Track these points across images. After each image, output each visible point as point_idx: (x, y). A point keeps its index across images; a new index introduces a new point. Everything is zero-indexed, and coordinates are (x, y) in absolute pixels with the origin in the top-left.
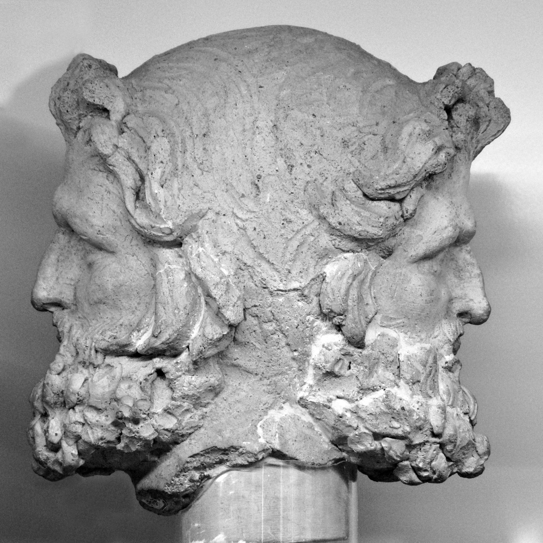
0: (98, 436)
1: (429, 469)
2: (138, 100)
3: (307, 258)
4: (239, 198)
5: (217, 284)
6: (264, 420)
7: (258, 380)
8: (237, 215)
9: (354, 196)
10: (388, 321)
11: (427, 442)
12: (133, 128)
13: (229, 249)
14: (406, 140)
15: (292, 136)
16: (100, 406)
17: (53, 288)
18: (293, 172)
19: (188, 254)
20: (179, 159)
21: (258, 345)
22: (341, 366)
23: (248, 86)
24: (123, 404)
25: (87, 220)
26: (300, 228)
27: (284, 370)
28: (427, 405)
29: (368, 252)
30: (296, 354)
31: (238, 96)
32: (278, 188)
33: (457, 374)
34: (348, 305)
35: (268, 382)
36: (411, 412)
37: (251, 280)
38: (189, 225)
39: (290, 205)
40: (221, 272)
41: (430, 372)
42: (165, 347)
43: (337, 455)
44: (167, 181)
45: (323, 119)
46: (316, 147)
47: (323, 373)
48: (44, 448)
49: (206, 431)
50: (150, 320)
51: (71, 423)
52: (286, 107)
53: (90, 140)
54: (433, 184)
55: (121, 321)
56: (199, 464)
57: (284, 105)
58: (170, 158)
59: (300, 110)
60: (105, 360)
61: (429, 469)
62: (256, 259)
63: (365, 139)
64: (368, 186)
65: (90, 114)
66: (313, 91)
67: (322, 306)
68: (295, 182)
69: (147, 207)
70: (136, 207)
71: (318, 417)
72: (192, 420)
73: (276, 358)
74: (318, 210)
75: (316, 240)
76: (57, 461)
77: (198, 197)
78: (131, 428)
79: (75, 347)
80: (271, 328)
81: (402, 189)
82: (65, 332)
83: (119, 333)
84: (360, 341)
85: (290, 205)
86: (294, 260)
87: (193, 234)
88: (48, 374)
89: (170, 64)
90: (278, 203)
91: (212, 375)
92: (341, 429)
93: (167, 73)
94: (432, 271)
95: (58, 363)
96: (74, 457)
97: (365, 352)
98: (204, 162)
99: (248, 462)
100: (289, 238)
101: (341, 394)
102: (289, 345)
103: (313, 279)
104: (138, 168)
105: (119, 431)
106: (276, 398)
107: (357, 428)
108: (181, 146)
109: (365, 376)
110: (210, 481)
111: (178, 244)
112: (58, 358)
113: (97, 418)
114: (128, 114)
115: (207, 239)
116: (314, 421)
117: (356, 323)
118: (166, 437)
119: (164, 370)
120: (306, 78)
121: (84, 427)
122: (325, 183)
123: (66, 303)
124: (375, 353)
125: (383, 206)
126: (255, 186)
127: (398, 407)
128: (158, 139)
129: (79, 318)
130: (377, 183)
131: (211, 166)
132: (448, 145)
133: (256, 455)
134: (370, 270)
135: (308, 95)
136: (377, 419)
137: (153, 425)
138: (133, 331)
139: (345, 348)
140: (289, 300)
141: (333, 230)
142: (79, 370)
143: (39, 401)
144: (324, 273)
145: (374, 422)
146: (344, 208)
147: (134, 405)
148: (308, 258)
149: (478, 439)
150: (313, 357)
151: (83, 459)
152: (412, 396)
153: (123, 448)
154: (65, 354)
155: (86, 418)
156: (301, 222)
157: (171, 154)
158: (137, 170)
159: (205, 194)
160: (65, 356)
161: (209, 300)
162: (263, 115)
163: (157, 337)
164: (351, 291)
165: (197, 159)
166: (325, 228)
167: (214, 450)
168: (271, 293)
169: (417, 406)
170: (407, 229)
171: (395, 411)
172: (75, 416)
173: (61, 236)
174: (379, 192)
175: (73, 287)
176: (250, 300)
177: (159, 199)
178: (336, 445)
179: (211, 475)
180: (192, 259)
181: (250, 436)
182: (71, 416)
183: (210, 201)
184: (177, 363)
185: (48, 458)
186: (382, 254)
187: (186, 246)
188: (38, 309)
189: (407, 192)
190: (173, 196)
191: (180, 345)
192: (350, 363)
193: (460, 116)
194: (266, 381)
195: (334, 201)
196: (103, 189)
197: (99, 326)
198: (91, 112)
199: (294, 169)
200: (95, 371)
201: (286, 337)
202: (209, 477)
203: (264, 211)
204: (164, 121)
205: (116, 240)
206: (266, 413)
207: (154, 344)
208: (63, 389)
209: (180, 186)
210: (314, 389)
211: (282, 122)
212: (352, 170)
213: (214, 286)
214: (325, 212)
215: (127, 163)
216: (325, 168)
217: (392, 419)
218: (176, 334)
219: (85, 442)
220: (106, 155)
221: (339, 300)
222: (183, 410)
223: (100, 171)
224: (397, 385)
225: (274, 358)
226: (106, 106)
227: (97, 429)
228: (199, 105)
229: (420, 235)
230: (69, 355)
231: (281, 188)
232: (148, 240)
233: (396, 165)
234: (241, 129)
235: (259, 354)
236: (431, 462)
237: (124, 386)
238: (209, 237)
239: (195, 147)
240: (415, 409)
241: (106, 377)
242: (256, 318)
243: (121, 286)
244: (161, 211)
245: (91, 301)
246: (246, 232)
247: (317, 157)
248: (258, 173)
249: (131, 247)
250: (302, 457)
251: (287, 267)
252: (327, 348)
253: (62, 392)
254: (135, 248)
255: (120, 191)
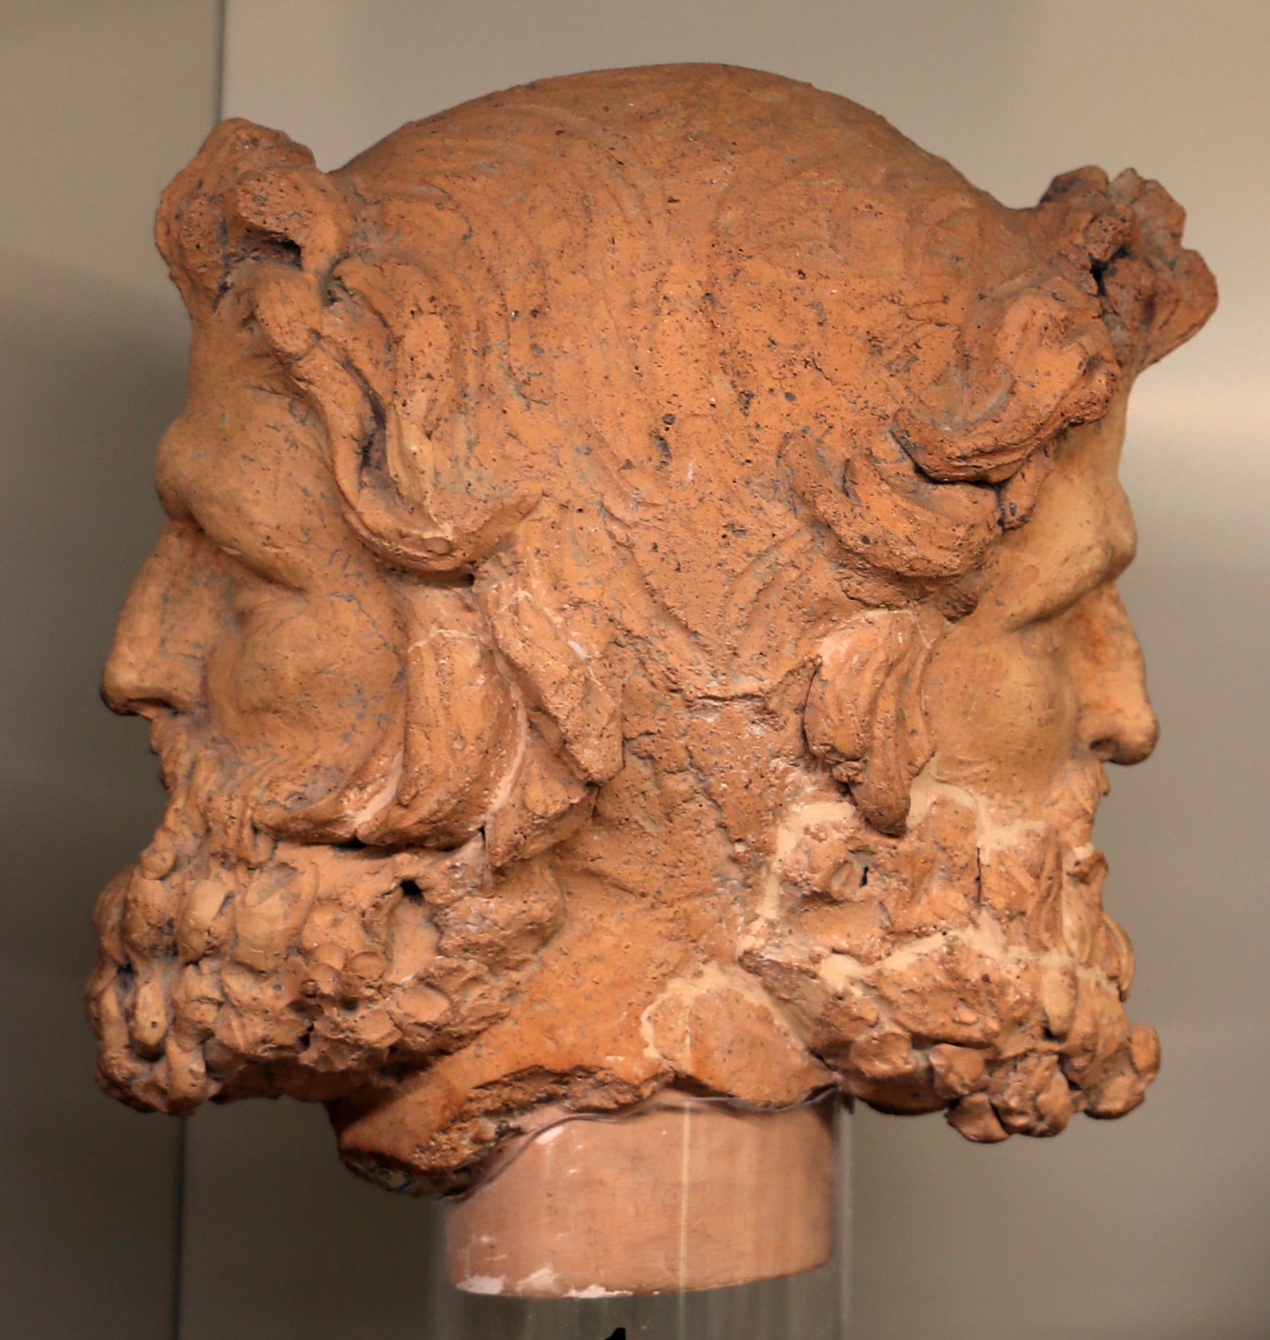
0: (254, 1034)
1: (1030, 1111)
2: (370, 223)
3: (779, 621)
4: (619, 471)
5: (562, 682)
6: (658, 1002)
7: (645, 909)
8: (613, 511)
9: (893, 473)
10: (954, 771)
11: (1033, 1050)
12: (358, 291)
13: (590, 594)
14: (1014, 340)
15: (752, 323)
16: (261, 966)
17: (151, 665)
18: (751, 410)
19: (490, 605)
20: (471, 370)
21: (650, 828)
22: (847, 879)
23: (642, 196)
24: (319, 965)
25: (238, 510)
26: (765, 547)
27: (709, 886)
28: (1037, 967)
29: (919, 608)
30: (740, 848)
31: (618, 220)
32: (715, 449)
33: (1095, 887)
34: (872, 737)
35: (669, 912)
36: (1003, 986)
37: (641, 671)
38: (495, 532)
39: (742, 490)
40: (571, 651)
41: (1049, 890)
42: (425, 829)
43: (820, 1078)
44: (441, 423)
45: (822, 282)
46: (806, 351)
47: (804, 896)
48: (124, 1051)
49: (517, 1028)
50: (389, 761)
51: (189, 1001)
52: (735, 251)
53: (252, 317)
54: (1065, 444)
55: (317, 758)
56: (498, 1105)
57: (727, 247)
58: (449, 366)
59: (769, 260)
60: (277, 851)
61: (1030, 1111)
62: (654, 621)
63: (919, 334)
64: (930, 449)
65: (254, 254)
66: (796, 216)
67: (809, 735)
68: (755, 433)
69: (388, 486)
70: (362, 485)
71: (784, 995)
72: (484, 1002)
73: (691, 857)
74: (812, 505)
75: (804, 578)
76: (153, 1086)
77: (516, 465)
78: (339, 1019)
79: (204, 815)
80: (683, 787)
81: (1006, 459)
82: (179, 777)
83: (311, 786)
84: (897, 821)
85: (742, 490)
86: (747, 625)
87: (502, 554)
88: (137, 877)
89: (448, 142)
90: (713, 486)
91: (537, 896)
92: (837, 1024)
93: (440, 161)
94: (1050, 649)
95: (162, 851)
96: (197, 1079)
97: (905, 846)
98: (533, 378)
99: (617, 1102)
100: (738, 570)
101: (844, 944)
102: (725, 827)
103: (791, 672)
104: (370, 388)
105: (307, 1023)
106: (686, 951)
107: (876, 1023)
108: (477, 338)
109: (900, 903)
110: (522, 1140)
111: (465, 578)
112: (162, 840)
113: (255, 992)
114: (347, 256)
115: (537, 569)
116: (775, 1004)
117: (891, 779)
118: (420, 1041)
119: (421, 884)
120: (780, 184)
121: (222, 1010)
122: (827, 440)
123: (183, 702)
124: (927, 847)
125: (960, 496)
126: (658, 442)
127: (975, 976)
128: (422, 319)
129: (214, 740)
130: (952, 443)
131: (550, 388)
132: (1108, 355)
133: (637, 1088)
134: (922, 648)
135: (786, 223)
136: (924, 1002)
137: (390, 1014)
138: (348, 787)
139: (859, 836)
140: (730, 720)
141: (845, 555)
142: (213, 874)
143: (114, 935)
144: (819, 656)
145: (918, 1010)
146: (875, 503)
147: (345, 966)
148: (782, 621)
149: (1138, 1037)
150: (780, 855)
151: (216, 1079)
152: (1005, 949)
153: (316, 1062)
154: (177, 829)
155: (226, 990)
156: (769, 532)
157: (451, 356)
158: (366, 394)
159: (535, 458)
160: (175, 838)
161: (539, 719)
162: (679, 268)
163: (406, 806)
164: (881, 702)
165: (515, 370)
166: (826, 549)
167: (536, 1072)
168: (689, 704)
169: (1016, 970)
170: (1005, 553)
171: (968, 986)
172: (201, 983)
173: (173, 540)
174: (957, 464)
175: (199, 664)
176: (636, 718)
177: (422, 467)
178: (820, 1057)
179: (524, 1127)
180: (500, 617)
181: (623, 1042)
182: (190, 984)
183: (547, 475)
184: (454, 867)
185: (133, 1076)
186: (950, 612)
187: (482, 583)
188: (115, 711)
189: (1015, 467)
190: (454, 460)
191: (464, 827)
192: (866, 870)
193: (1122, 287)
194: (665, 912)
195: (848, 484)
196: (281, 435)
197: (264, 764)
198: (256, 250)
199: (754, 402)
200: (251, 876)
201: (719, 808)
202: (518, 1132)
203: (679, 504)
204: (434, 278)
205: (309, 561)
206: (662, 986)
207: (400, 822)
208: (173, 915)
209: (472, 437)
210: (778, 931)
211: (725, 285)
212: (891, 408)
213: (554, 687)
214: (830, 511)
215: (343, 375)
216: (826, 403)
217: (960, 1003)
218: (454, 801)
219: (223, 1046)
220: (290, 354)
221: (854, 724)
222: (464, 978)
223: (274, 392)
224: (974, 923)
225: (688, 857)
226: (293, 237)
227: (254, 1016)
228: (521, 240)
229: (1033, 566)
230: (188, 832)
231: (723, 447)
232: (389, 566)
233: (992, 401)
234: (627, 300)
235: (652, 847)
236: (1037, 1094)
237: (322, 919)
238: (542, 564)
239: (511, 341)
240: (1012, 978)
241: (277, 896)
242: (648, 761)
243: (319, 672)
244: (424, 498)
245: (239, 705)
246: (632, 553)
247: (809, 375)
248: (666, 411)
249: (344, 580)
250: (744, 1090)
251: (729, 641)
252: (815, 836)
253: (170, 923)
254: (353, 581)
255: (323, 444)
